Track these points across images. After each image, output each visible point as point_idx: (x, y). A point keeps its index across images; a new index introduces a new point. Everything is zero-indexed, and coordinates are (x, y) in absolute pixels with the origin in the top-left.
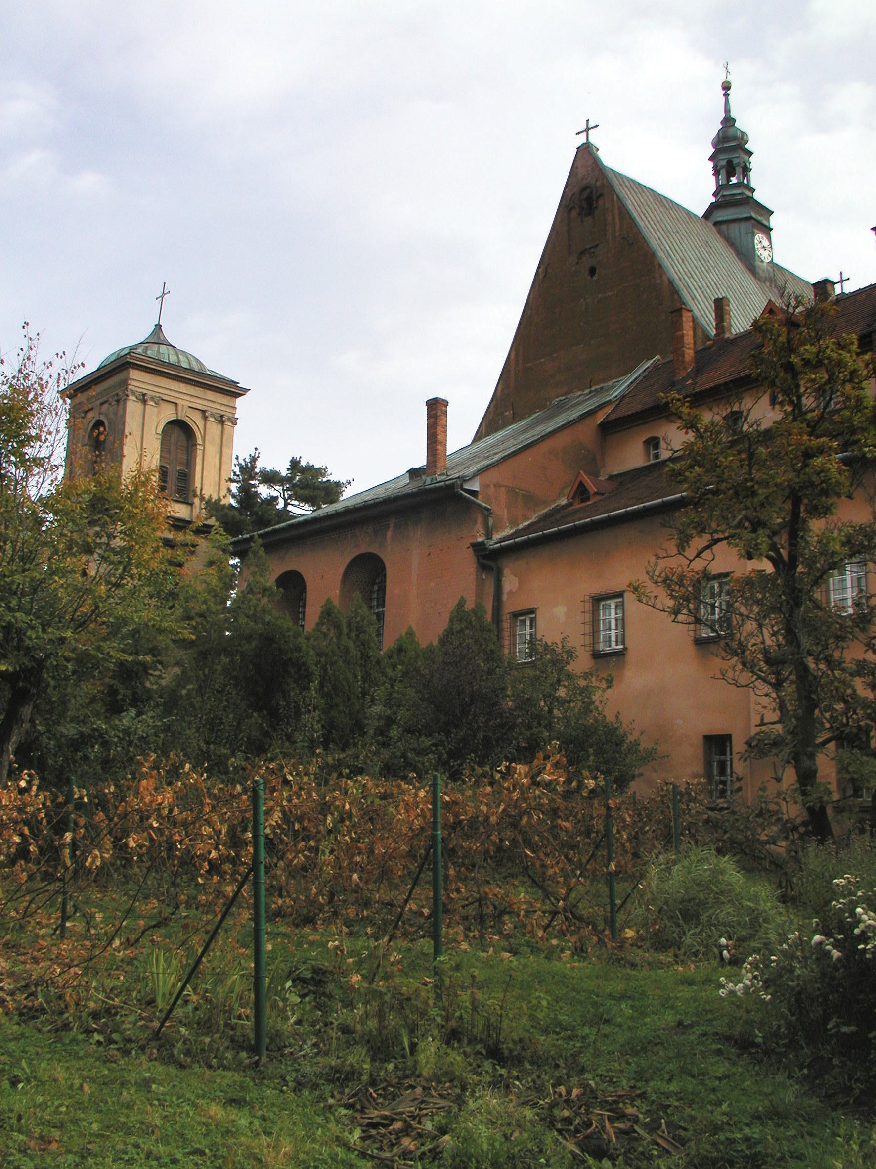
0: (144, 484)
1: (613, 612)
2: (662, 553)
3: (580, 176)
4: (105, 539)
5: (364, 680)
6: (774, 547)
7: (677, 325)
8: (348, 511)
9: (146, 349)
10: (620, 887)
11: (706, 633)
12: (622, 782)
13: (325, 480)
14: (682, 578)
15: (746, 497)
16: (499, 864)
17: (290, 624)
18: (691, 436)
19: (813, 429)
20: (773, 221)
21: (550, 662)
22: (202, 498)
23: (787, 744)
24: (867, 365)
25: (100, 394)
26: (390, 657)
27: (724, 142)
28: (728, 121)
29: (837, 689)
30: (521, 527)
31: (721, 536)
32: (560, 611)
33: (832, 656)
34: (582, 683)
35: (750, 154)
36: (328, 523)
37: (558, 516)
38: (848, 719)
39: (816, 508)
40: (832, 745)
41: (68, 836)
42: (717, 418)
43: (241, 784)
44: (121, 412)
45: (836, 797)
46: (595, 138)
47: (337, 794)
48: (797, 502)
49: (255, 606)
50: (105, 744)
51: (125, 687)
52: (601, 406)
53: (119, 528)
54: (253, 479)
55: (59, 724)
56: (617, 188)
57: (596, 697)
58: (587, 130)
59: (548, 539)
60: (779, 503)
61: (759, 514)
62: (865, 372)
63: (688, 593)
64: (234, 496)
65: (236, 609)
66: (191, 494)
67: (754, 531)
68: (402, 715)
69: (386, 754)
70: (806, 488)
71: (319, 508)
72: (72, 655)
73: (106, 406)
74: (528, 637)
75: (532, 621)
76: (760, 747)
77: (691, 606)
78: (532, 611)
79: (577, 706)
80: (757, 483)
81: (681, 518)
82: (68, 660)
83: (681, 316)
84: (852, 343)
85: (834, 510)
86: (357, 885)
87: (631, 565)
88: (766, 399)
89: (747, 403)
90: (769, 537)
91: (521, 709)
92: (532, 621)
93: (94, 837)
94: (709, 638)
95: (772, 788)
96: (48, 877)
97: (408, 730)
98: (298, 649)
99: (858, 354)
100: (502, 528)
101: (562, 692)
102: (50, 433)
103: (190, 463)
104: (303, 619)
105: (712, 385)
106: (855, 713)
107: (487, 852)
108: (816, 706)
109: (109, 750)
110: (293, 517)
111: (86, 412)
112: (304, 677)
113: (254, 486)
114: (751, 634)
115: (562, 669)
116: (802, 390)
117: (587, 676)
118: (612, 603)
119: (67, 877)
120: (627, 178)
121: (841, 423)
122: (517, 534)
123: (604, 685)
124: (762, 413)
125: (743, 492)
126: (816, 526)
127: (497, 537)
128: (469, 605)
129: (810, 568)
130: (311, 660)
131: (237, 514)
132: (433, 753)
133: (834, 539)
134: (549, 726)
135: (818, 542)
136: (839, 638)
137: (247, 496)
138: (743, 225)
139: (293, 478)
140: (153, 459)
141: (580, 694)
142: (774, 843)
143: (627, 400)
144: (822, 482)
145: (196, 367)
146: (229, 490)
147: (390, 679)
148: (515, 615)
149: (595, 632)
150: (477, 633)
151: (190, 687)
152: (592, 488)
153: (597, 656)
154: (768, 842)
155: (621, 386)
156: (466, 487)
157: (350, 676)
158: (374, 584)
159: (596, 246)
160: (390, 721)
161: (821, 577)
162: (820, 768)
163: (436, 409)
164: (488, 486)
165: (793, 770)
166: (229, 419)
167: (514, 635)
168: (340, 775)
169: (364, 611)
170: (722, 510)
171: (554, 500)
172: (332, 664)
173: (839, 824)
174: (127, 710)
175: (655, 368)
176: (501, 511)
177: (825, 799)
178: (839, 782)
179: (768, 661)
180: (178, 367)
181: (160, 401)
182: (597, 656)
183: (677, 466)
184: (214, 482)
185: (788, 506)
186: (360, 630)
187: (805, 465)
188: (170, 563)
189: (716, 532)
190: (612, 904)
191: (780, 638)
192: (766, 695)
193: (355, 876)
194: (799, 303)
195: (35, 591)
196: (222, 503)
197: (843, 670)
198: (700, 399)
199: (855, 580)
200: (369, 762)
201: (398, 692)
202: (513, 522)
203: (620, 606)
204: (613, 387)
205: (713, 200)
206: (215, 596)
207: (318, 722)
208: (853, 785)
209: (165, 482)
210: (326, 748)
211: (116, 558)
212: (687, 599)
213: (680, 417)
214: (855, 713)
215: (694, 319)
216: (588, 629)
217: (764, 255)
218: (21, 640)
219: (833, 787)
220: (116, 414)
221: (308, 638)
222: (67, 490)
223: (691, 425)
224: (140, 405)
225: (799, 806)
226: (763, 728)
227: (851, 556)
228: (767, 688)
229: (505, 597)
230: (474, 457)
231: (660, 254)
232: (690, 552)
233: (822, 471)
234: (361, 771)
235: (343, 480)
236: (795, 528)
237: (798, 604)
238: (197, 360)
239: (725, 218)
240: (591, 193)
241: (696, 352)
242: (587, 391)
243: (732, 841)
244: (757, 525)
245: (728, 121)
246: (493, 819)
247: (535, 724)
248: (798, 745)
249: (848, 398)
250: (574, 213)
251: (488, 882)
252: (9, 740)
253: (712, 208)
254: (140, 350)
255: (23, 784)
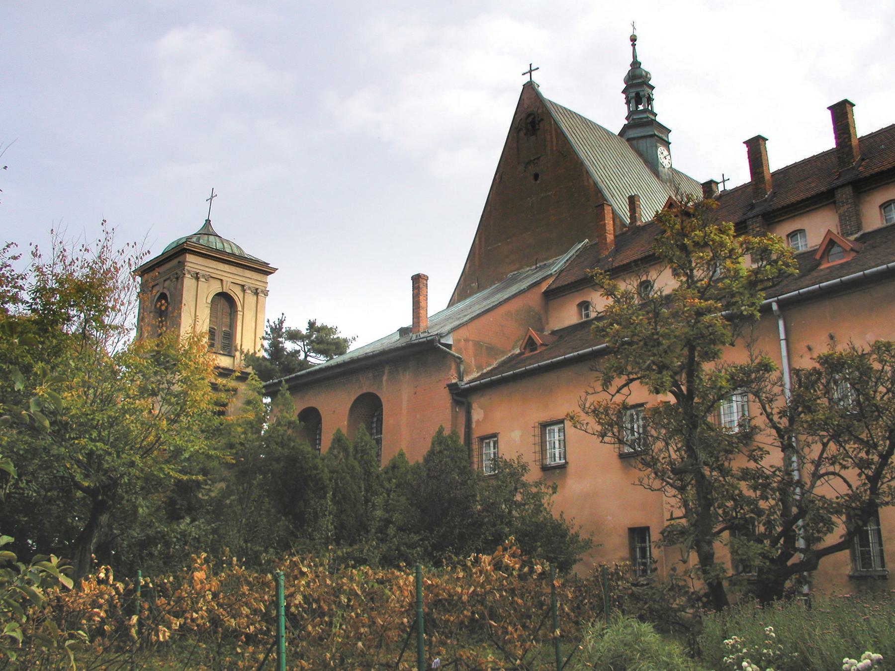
0: (196, 343)
1: (556, 435)
2: (590, 391)
3: (526, 106)
4: (165, 386)
5: (367, 491)
6: (676, 384)
7: (601, 216)
8: (353, 361)
9: (199, 239)
10: (563, 647)
11: (627, 450)
12: (564, 566)
13: (335, 337)
14: (606, 409)
15: (654, 346)
16: (472, 631)
17: (310, 449)
18: (610, 301)
19: (703, 294)
20: (671, 137)
21: (509, 474)
22: (242, 352)
23: (690, 534)
24: (741, 245)
25: (163, 275)
26: (386, 473)
27: (633, 80)
28: (636, 64)
29: (727, 491)
30: (485, 371)
31: (635, 376)
32: (516, 435)
33: (723, 465)
34: (534, 490)
35: (652, 88)
36: (339, 370)
37: (513, 362)
38: (736, 513)
39: (706, 353)
40: (726, 534)
41: (135, 618)
42: (630, 287)
43: (271, 573)
44: (179, 286)
45: (730, 572)
46: (536, 77)
47: (345, 580)
48: (692, 349)
49: (283, 435)
50: (167, 544)
51: (181, 500)
52: (545, 279)
53: (177, 378)
54: (281, 336)
55: (130, 528)
56: (554, 113)
57: (544, 501)
58: (530, 72)
59: (509, 379)
60: (678, 351)
61: (663, 359)
62: (740, 251)
63: (612, 421)
64: (266, 350)
65: (269, 437)
66: (233, 349)
67: (660, 372)
68: (396, 516)
69: (384, 548)
70: (699, 338)
71: (332, 358)
72: (142, 475)
73: (168, 282)
74: (492, 456)
75: (495, 443)
76: (671, 536)
77: (615, 430)
78: (495, 435)
79: (530, 508)
80: (662, 336)
81: (604, 363)
82: (138, 478)
83: (604, 209)
84: (730, 229)
85: (721, 355)
86: (362, 651)
87: (569, 399)
88: (668, 272)
89: (653, 275)
90: (671, 376)
91: (487, 511)
92: (495, 443)
93: (157, 618)
94: (629, 453)
95: (681, 568)
96: (119, 649)
97: (400, 529)
98: (316, 467)
99: (734, 237)
100: (471, 372)
101: (518, 498)
102: (123, 304)
103: (232, 325)
104: (320, 444)
105: (628, 261)
106: (742, 508)
107: (462, 623)
108: (712, 505)
109: (169, 548)
110: (311, 366)
111: (153, 287)
112: (321, 490)
113: (281, 342)
114: (661, 451)
115: (518, 480)
116: (693, 265)
117: (537, 484)
118: (556, 428)
119: (134, 649)
120: (561, 107)
121: (724, 289)
122: (483, 376)
123: (550, 491)
124: (665, 282)
125: (652, 342)
126: (708, 367)
127: (466, 379)
128: (447, 432)
129: (704, 399)
130: (326, 475)
131: (268, 364)
132: (420, 546)
133: (721, 377)
134: (509, 524)
135: (709, 379)
136: (728, 452)
137: (276, 350)
138: (649, 141)
139: (311, 336)
140: (204, 326)
141: (533, 498)
142: (683, 611)
143: (564, 274)
144: (711, 334)
145: (237, 252)
146: (262, 346)
147: (387, 490)
148: (482, 439)
149: (543, 451)
150: (452, 454)
151: (233, 498)
152: (538, 340)
153: (545, 468)
154: (679, 610)
155: (559, 263)
156: (443, 341)
157: (355, 488)
158: (373, 416)
159: (538, 158)
160: (387, 522)
161: (712, 406)
162: (716, 551)
163: (419, 282)
164: (460, 340)
165: (696, 554)
166: (262, 291)
167: (482, 455)
168: (347, 566)
169: (367, 438)
170: (635, 357)
171: (510, 351)
172: (342, 479)
173: (734, 596)
174: (183, 518)
175: (585, 248)
176: (469, 358)
177: (721, 575)
178: (733, 560)
179: (674, 471)
180: (223, 252)
181: (208, 278)
182: (545, 468)
183: (601, 324)
184: (251, 339)
185: (686, 352)
186: (364, 452)
187: (697, 322)
188: (216, 403)
189: (631, 373)
190: (558, 661)
191: (683, 452)
192: (674, 496)
193: (360, 644)
194: (689, 199)
195: (111, 426)
196: (257, 355)
197: (732, 476)
198: (617, 272)
199: (740, 406)
200: (370, 554)
201: (393, 500)
202: (479, 368)
203: (562, 430)
204: (553, 263)
205: (626, 122)
206: (252, 428)
207: (332, 524)
208: (742, 564)
209: (213, 340)
210: (338, 544)
211: (173, 400)
212: (611, 425)
213: (602, 287)
214: (742, 508)
215: (614, 212)
216: (538, 448)
217: (665, 162)
218: (100, 464)
219: (728, 565)
220: (176, 288)
221: (323, 459)
222: (138, 346)
223: (610, 293)
224: (194, 281)
225: (702, 581)
226: (672, 522)
227: (734, 389)
228: (674, 492)
229: (474, 425)
230: (448, 318)
231: (587, 163)
232: (613, 389)
233: (711, 326)
234: (364, 562)
235: (349, 337)
236: (691, 369)
237: (695, 427)
238: (238, 247)
239: (636, 135)
240: (534, 118)
241: (616, 237)
242: (534, 267)
243: (651, 610)
244: (662, 368)
245: (636, 64)
246: (465, 598)
247: (499, 522)
248: (697, 533)
249: (729, 270)
250: (522, 134)
251: (463, 647)
252: (91, 541)
253: (626, 128)
254: (194, 240)
255: (102, 575)
